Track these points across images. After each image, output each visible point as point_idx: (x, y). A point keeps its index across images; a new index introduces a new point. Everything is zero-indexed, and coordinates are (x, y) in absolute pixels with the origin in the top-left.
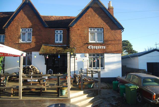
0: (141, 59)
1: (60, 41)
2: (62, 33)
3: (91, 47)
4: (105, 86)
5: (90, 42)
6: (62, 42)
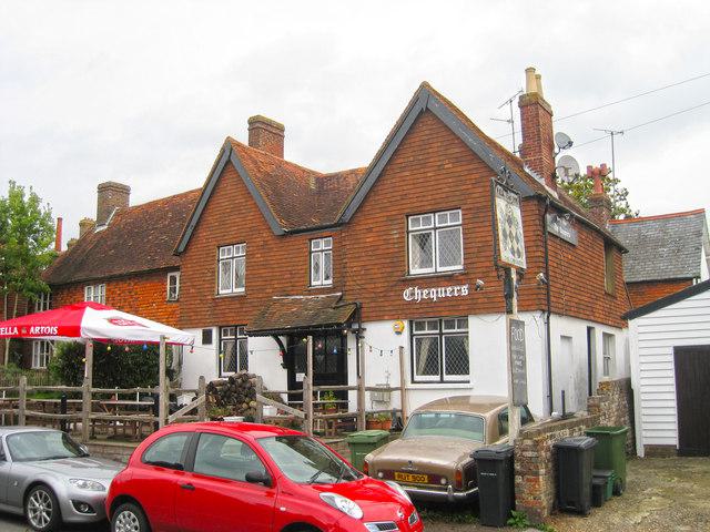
0: (642, 330)
1: (327, 278)
2: (460, 222)
3: (413, 294)
4: (115, 472)
5: (415, 271)
6: (330, 281)
